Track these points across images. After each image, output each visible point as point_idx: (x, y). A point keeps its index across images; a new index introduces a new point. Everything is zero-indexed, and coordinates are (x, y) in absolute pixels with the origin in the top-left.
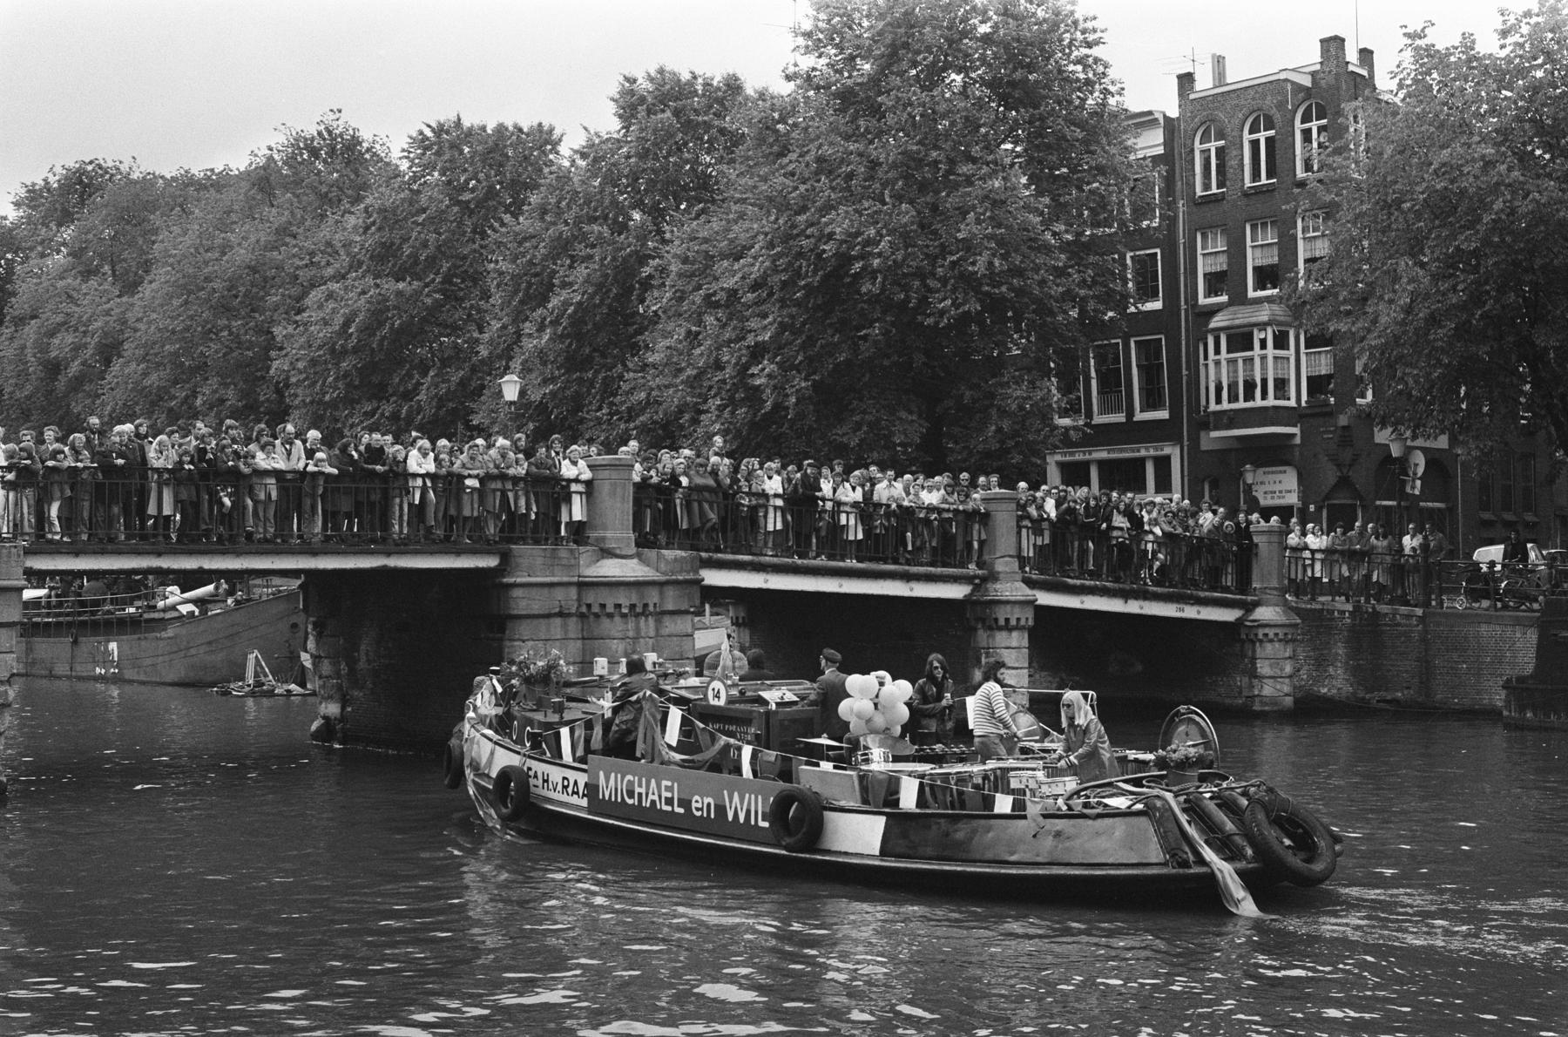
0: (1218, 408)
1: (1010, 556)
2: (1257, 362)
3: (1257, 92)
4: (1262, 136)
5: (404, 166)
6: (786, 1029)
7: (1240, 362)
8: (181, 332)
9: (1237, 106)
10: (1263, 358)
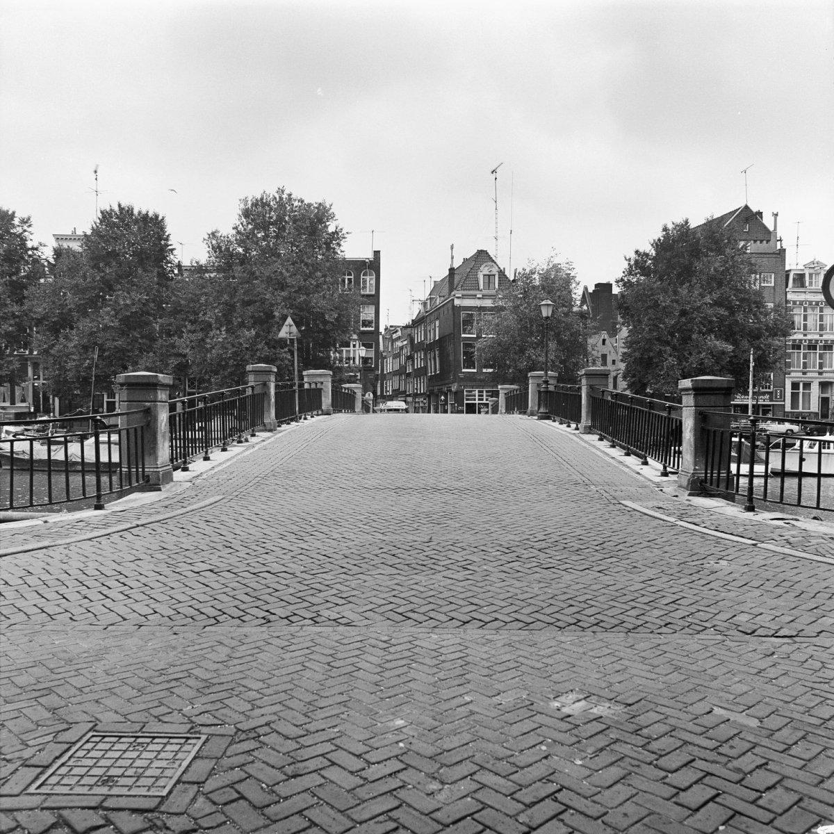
2: (352, 351)
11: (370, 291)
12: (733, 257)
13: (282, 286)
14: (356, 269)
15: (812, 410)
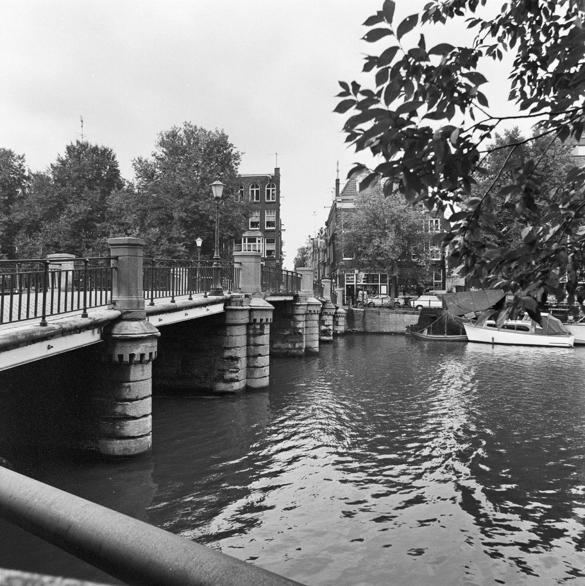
1: (134, 418)
2: (257, 246)
5: (51, 176)
6: (517, 506)
10: (259, 245)
11: (272, 199)
12: (553, 157)
13: (181, 195)
14: (261, 183)
15: (274, 249)
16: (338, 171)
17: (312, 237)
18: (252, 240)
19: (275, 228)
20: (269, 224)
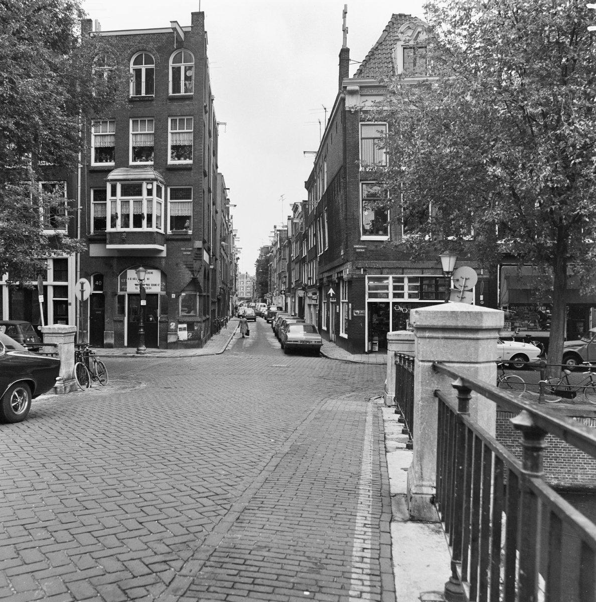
0: (113, 230)
2: (145, 203)
3: (142, 39)
4: (143, 68)
7: (131, 203)
8: (378, 102)
9: (127, 45)
10: (150, 201)
14: (159, 49)
16: (345, 31)
17: (277, 228)
18: (132, 188)
19: (191, 162)
20: (179, 151)
